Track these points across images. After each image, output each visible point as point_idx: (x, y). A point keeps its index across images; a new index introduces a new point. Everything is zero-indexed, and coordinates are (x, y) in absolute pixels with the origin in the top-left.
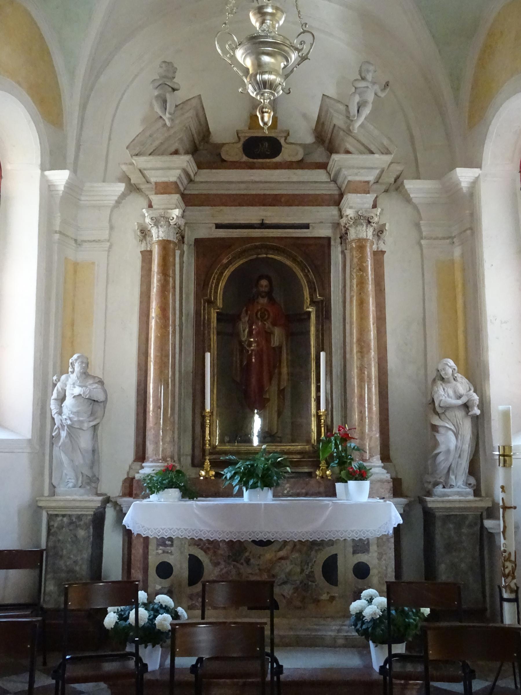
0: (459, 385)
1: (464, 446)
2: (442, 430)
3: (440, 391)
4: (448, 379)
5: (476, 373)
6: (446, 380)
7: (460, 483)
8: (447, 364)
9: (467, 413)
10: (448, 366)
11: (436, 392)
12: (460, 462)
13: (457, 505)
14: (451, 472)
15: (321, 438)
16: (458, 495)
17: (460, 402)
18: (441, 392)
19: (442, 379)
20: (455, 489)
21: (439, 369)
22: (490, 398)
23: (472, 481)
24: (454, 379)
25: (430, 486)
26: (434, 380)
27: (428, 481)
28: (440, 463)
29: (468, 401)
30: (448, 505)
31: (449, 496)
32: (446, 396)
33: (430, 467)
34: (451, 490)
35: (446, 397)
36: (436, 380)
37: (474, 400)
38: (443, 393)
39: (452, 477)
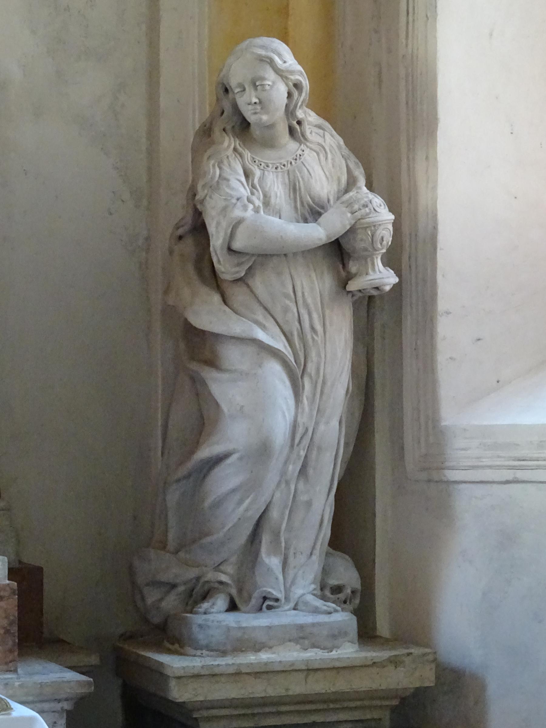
0: (309, 157)
1: (322, 427)
2: (233, 356)
3: (234, 183)
4: (271, 127)
5: (378, 105)
6: (255, 131)
7: (305, 587)
8: (271, 63)
9: (343, 283)
10: (278, 71)
11: (215, 187)
12: (303, 498)
13: (298, 687)
14: (266, 538)
15: (165, 642)
16: (296, 640)
17: (317, 233)
18: (238, 187)
19: (243, 127)
20: (284, 617)
21: (233, 82)
22: (435, 217)
23: (347, 575)
24: (292, 131)
25: (171, 602)
26: (206, 132)
27: (164, 577)
28: (218, 504)
29: (352, 231)
30: (259, 689)
31: (258, 647)
32: (258, 203)
33: (172, 520)
34: (264, 620)
35: (256, 210)
36: (217, 132)
37: (375, 226)
38: (244, 191)
39: (272, 562)
